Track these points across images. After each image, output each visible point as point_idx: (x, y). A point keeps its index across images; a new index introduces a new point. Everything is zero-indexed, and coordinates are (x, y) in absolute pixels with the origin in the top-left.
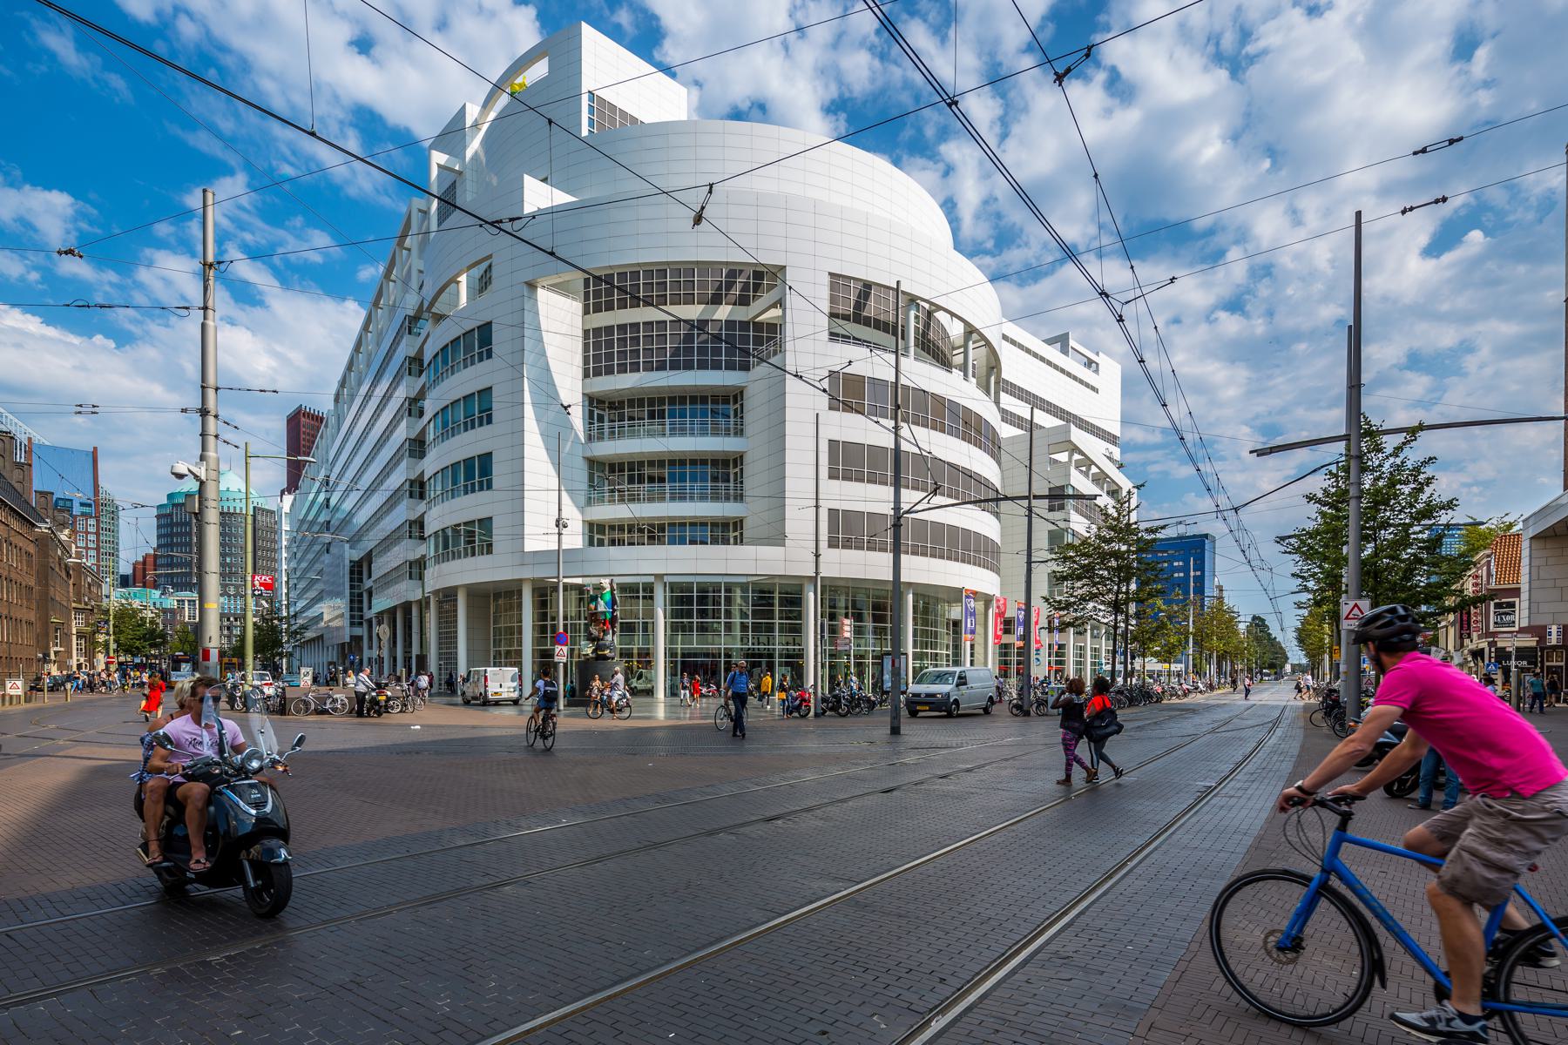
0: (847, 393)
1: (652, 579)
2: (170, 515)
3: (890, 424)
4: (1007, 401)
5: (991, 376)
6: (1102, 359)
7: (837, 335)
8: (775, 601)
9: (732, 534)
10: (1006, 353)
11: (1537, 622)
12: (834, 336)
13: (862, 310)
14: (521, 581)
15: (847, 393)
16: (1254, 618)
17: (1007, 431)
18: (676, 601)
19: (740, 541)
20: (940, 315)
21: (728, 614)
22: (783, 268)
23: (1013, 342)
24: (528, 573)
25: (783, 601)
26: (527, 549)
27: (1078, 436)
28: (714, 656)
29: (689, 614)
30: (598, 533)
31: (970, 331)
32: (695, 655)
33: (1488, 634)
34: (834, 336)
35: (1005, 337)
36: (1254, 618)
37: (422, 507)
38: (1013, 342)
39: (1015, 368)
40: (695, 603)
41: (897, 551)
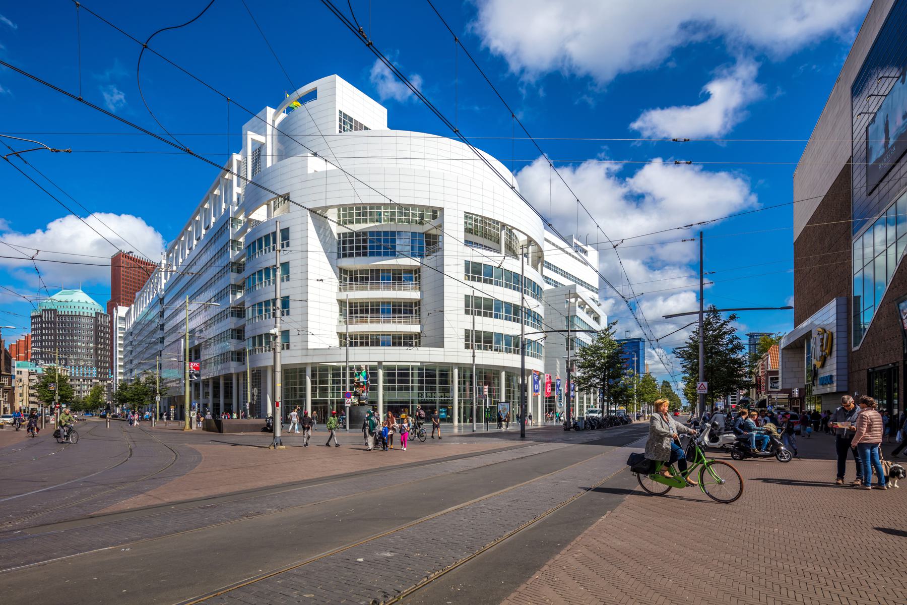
0: (475, 271)
1: (376, 364)
2: (41, 316)
3: (525, 305)
4: (547, 272)
5: (539, 260)
6: (589, 248)
7: (471, 242)
8: (436, 376)
9: (414, 341)
10: (546, 247)
11: (788, 387)
12: (468, 243)
13: (481, 231)
14: (306, 364)
15: (475, 271)
16: (664, 382)
17: (546, 287)
18: (389, 375)
19: (418, 344)
20: (514, 231)
21: (344, 382)
22: (442, 209)
23: (550, 242)
24: (309, 360)
25: (441, 375)
26: (311, 346)
27: (580, 290)
28: (432, 403)
29: (393, 381)
30: (349, 340)
31: (530, 241)
32: (397, 403)
33: (768, 392)
34: (468, 243)
35: (546, 240)
36: (664, 382)
37: (241, 322)
38: (550, 242)
39: (551, 255)
40: (398, 376)
41: (523, 355)
